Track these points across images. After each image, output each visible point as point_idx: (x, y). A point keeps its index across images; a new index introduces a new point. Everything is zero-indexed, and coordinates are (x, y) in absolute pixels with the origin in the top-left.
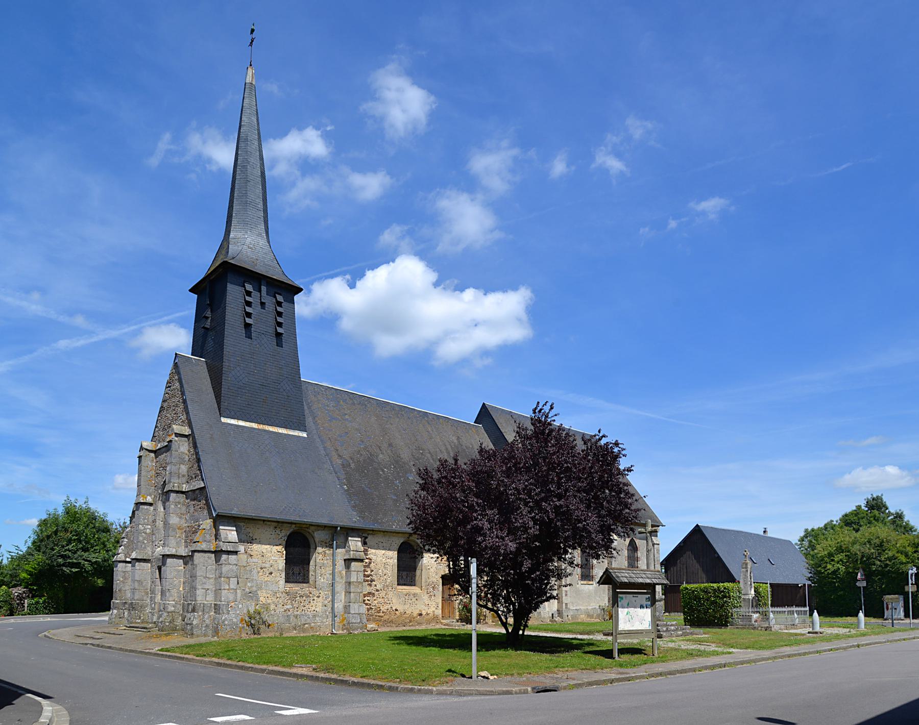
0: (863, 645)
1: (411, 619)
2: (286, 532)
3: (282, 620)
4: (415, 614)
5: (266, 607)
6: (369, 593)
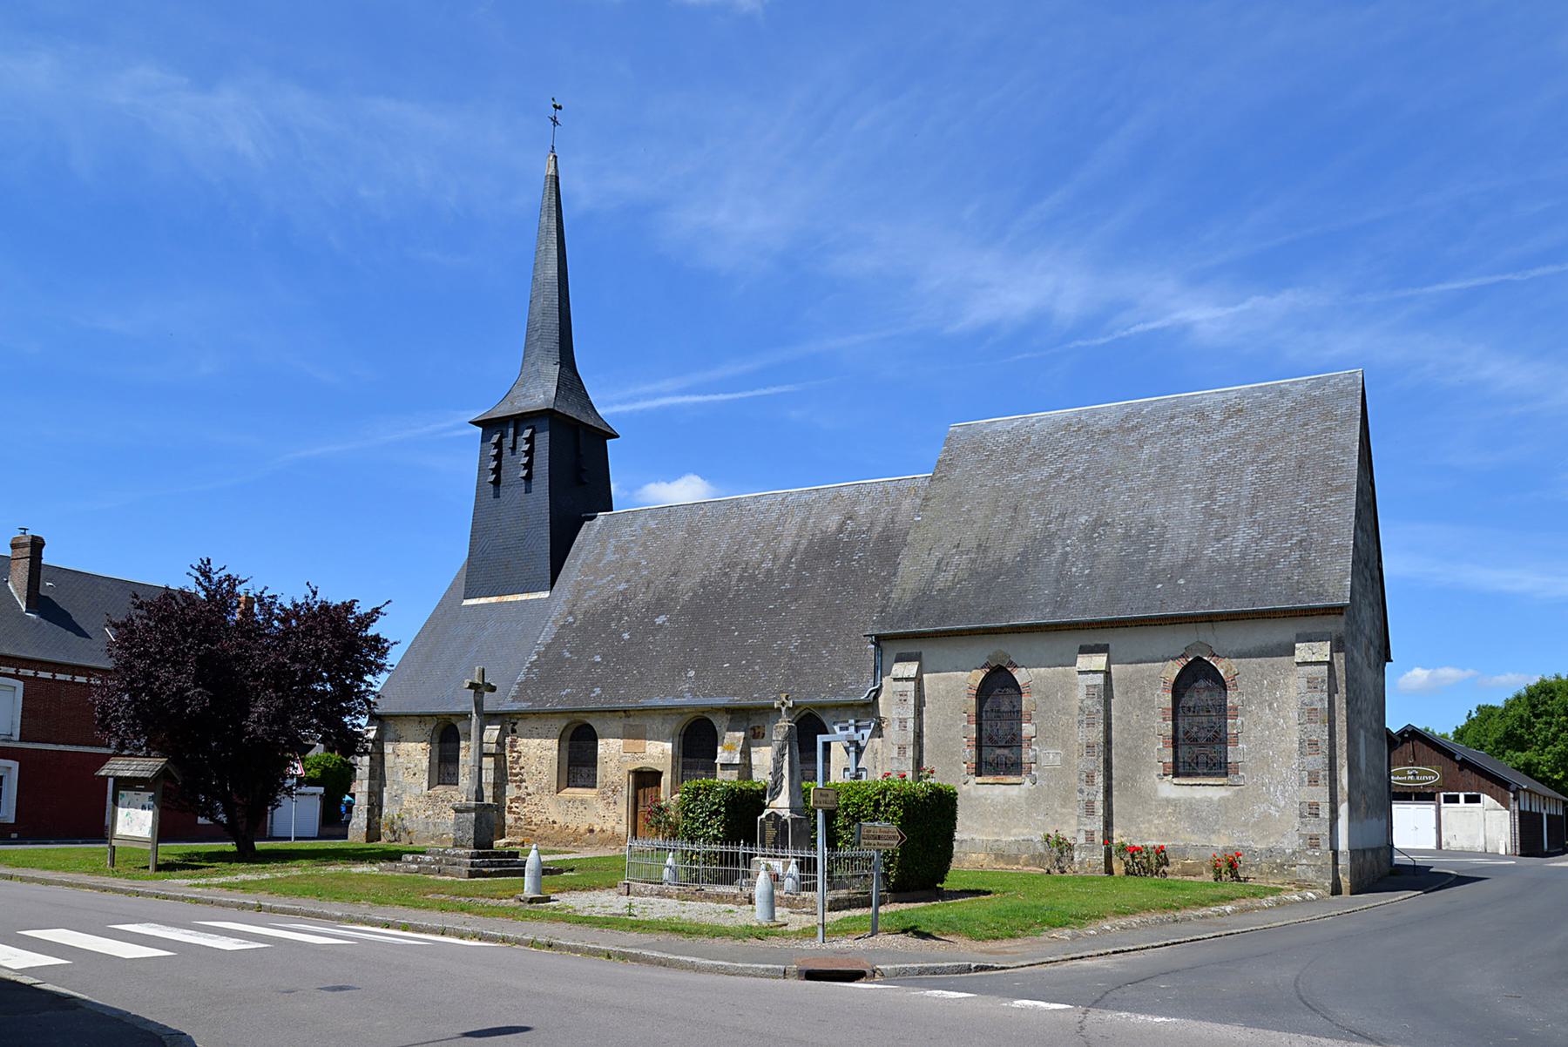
0: (560, 947)
1: (577, 839)
2: (674, 725)
3: (421, 828)
4: (583, 828)
5: (409, 811)
6: (518, 798)
